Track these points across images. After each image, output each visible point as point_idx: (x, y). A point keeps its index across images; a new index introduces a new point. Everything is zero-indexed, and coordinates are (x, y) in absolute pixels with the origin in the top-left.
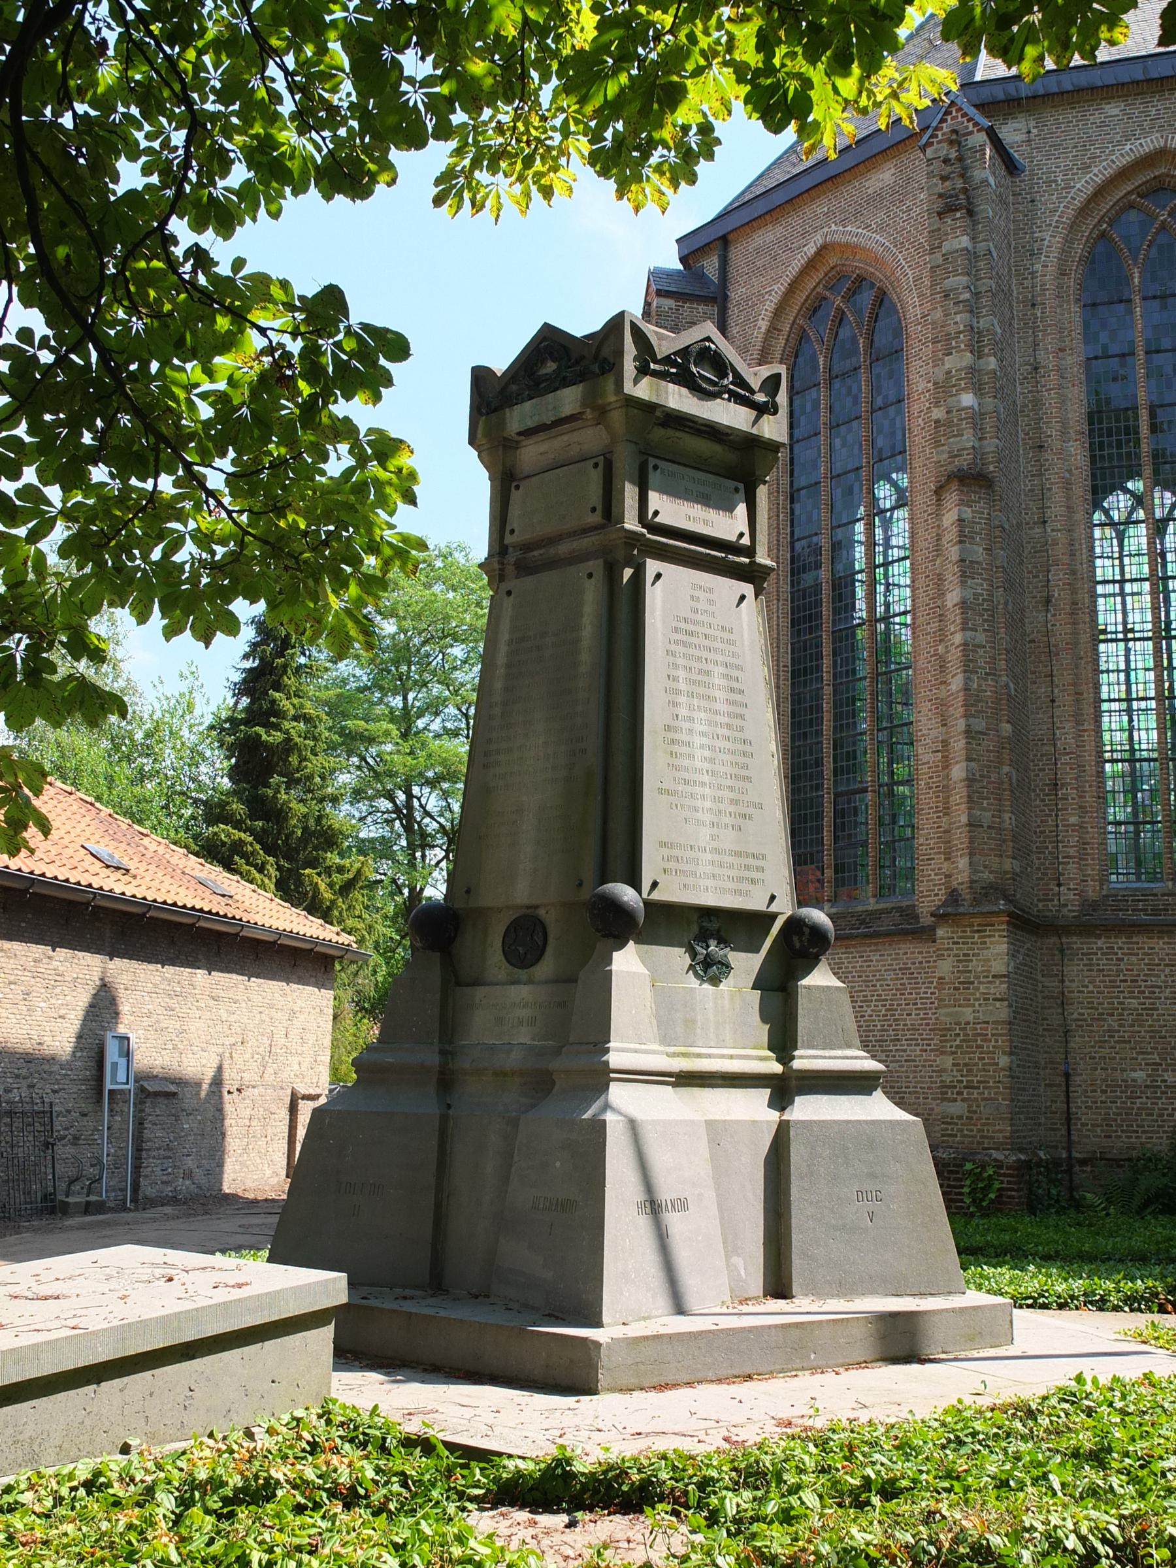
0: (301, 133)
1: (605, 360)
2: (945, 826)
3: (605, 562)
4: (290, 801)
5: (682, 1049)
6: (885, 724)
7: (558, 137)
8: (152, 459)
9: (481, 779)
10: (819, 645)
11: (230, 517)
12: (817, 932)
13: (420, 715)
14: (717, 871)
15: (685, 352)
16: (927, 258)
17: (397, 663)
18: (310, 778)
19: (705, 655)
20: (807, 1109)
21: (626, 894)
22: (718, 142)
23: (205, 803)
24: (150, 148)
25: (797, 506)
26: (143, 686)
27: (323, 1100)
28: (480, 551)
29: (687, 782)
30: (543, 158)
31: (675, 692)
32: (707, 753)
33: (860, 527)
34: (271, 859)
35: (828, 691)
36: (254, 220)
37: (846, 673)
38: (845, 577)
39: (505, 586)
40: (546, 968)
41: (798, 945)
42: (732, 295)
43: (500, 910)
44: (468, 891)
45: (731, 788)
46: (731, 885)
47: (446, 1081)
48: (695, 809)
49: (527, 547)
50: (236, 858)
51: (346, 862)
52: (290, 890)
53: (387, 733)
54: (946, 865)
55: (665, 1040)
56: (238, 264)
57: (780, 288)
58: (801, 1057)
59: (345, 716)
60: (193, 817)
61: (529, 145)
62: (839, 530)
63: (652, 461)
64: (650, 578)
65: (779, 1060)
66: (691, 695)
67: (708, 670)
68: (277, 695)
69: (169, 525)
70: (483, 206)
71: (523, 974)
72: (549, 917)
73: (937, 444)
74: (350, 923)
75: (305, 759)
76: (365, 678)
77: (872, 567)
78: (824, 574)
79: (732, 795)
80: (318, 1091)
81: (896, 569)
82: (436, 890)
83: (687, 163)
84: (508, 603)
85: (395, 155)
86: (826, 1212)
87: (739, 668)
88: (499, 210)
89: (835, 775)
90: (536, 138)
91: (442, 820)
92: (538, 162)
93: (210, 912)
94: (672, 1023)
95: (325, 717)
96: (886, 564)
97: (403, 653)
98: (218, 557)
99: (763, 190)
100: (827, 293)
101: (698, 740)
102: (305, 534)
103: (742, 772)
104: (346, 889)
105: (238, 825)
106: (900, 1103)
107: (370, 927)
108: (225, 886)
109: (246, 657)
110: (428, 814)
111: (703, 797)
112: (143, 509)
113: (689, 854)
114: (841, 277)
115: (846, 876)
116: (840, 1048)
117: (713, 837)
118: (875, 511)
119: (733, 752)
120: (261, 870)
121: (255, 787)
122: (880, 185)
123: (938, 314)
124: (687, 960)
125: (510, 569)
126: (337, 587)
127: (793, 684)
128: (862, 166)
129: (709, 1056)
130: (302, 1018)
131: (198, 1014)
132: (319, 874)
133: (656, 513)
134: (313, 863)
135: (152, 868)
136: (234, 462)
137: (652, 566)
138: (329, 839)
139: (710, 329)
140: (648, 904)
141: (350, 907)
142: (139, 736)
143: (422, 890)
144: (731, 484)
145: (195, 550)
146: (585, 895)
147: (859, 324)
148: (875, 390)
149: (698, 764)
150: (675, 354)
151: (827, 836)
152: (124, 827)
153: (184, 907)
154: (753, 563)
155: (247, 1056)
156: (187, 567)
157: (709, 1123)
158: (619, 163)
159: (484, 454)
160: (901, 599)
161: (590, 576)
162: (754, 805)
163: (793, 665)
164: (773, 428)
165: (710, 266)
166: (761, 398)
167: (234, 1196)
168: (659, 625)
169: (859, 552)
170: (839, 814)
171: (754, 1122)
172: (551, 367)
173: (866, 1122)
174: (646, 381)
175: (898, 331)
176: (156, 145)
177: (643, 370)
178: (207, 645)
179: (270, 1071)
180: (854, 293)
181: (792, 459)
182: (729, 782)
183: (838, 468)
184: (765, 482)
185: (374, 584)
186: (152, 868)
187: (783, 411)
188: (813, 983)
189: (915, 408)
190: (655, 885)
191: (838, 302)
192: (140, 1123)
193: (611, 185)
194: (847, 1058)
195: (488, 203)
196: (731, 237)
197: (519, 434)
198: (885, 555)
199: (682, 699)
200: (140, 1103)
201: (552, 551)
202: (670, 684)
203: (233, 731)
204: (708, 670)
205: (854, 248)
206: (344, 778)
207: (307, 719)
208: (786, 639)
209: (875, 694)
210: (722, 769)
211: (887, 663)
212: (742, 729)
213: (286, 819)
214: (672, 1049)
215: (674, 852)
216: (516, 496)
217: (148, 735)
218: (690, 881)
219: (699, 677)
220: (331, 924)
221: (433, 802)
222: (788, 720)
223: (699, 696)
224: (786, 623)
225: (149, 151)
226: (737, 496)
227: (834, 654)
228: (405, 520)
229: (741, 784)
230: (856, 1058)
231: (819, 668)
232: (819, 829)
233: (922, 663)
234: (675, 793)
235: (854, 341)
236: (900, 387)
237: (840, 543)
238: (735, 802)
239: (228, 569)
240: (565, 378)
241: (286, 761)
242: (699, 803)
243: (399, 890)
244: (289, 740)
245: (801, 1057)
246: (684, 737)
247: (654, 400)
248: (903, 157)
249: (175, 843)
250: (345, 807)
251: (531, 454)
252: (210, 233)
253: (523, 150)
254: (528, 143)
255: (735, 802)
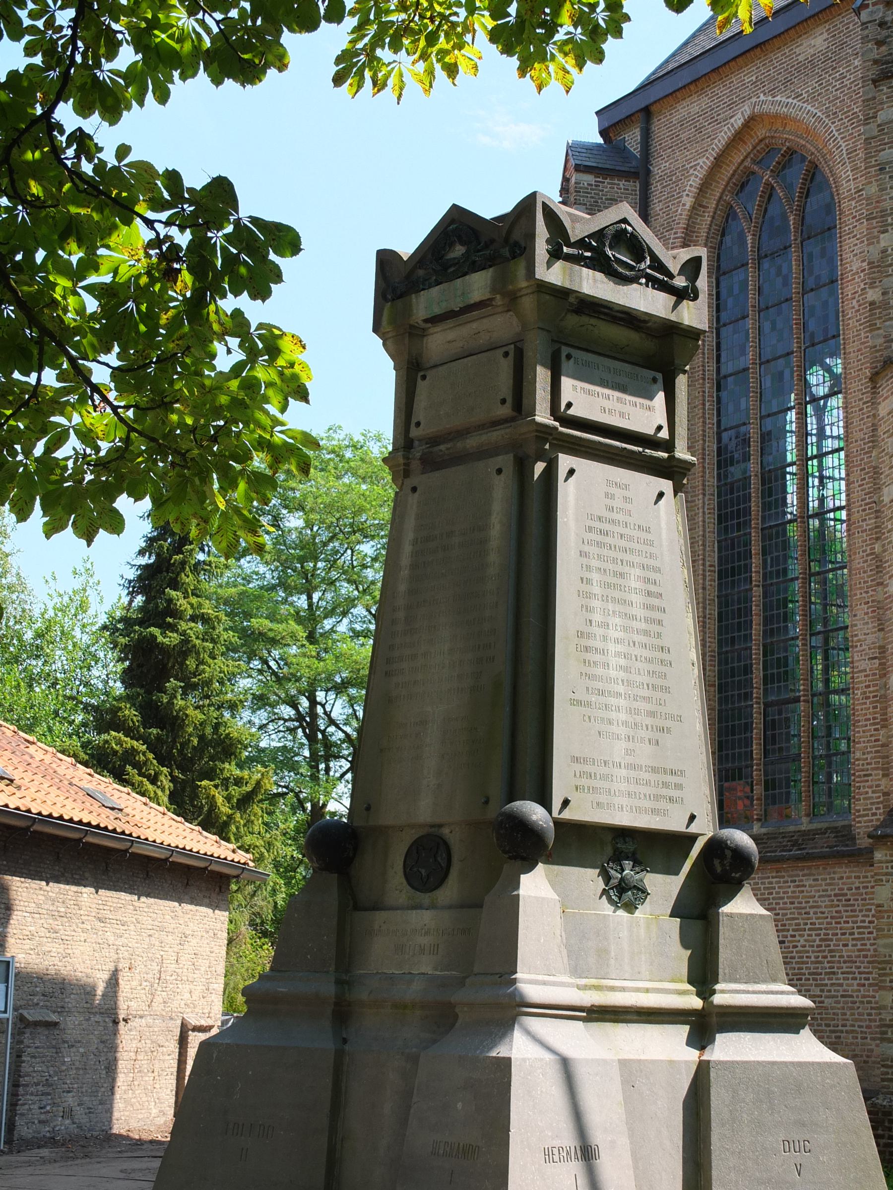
0: (191, 13)
1: (516, 244)
2: (883, 740)
3: (515, 456)
4: (187, 707)
5: (593, 981)
6: (819, 628)
7: (463, 13)
8: (36, 352)
9: (381, 685)
10: (748, 543)
11: (116, 413)
12: (739, 856)
13: (328, 614)
14: (632, 788)
15: (599, 235)
16: (862, 128)
17: (302, 560)
18: (208, 683)
19: (620, 555)
20: (729, 1048)
21: (536, 813)
22: (627, 18)
23: (96, 709)
24: (33, 26)
25: (724, 394)
26: (34, 583)
27: (214, 1031)
28: (388, 444)
29: (601, 693)
30: (447, 35)
31: (589, 596)
32: (622, 662)
33: (792, 416)
34: (165, 770)
35: (757, 592)
36: (141, 104)
37: (776, 574)
38: (776, 470)
39: (409, 483)
40: (449, 892)
41: (719, 869)
42: (655, 170)
43: (401, 829)
44: (368, 809)
45: (647, 699)
46: (648, 804)
47: (342, 1014)
48: (610, 722)
49: (434, 441)
50: (129, 768)
51: (246, 774)
52: (185, 803)
53: (293, 636)
54: (884, 782)
55: (576, 971)
56: (123, 151)
57: (705, 163)
58: (723, 992)
59: (248, 616)
60: (84, 724)
61: (432, 22)
62: (769, 420)
63: (565, 351)
64: (562, 473)
65: (699, 994)
66: (605, 599)
67: (625, 569)
68: (173, 593)
69: (52, 419)
70: (385, 85)
71: (425, 898)
72: (455, 837)
73: (872, 327)
74: (248, 840)
75: (202, 662)
76: (268, 576)
77: (804, 459)
78: (753, 467)
79: (649, 707)
80: (210, 1022)
81: (829, 461)
82: (339, 803)
83: (594, 41)
84: (413, 500)
85: (288, 39)
86: (750, 1163)
87: (657, 570)
88: (401, 89)
89: (765, 683)
90: (440, 14)
91: (348, 729)
92: (442, 39)
93: (98, 827)
94: (584, 953)
95: (224, 618)
96: (820, 456)
97: (310, 550)
98: (102, 453)
99: (676, 65)
100: (756, 168)
101: (612, 648)
102: (193, 430)
103: (659, 682)
104: (244, 802)
105: (130, 732)
106: (834, 1047)
107: (269, 844)
108: (115, 798)
109: (142, 552)
110: (332, 722)
111: (618, 709)
112: (26, 404)
113: (603, 770)
114: (771, 150)
115: (777, 791)
116: (764, 981)
117: (629, 752)
118: (806, 398)
119: (649, 661)
120: (154, 780)
121: (149, 692)
122: (812, 51)
123: (873, 189)
124: (601, 885)
125: (415, 465)
126: (225, 485)
127: (720, 585)
128: (792, 32)
129: (623, 989)
130: (194, 942)
131: (83, 936)
132: (216, 786)
133: (569, 405)
134: (210, 774)
135: (38, 778)
136: (119, 357)
137: (565, 461)
138: (227, 748)
139: (626, 210)
140: (558, 823)
141: (249, 823)
142: (29, 635)
143: (324, 805)
144: (651, 374)
145: (79, 446)
146: (492, 813)
147: (790, 200)
148: (806, 267)
149: (613, 673)
150: (589, 236)
151: (756, 749)
152: (9, 733)
153: (71, 820)
154: (672, 458)
155: (134, 983)
156: (70, 464)
157: (624, 1064)
158: (523, 39)
159: (389, 343)
160: (837, 493)
161: (499, 471)
162: (672, 717)
163: (720, 564)
164: (694, 315)
165: (632, 139)
166: (680, 282)
167: (121, 1136)
168: (572, 524)
169: (791, 441)
170: (769, 725)
171: (671, 1062)
172: (459, 251)
173: (792, 1063)
174: (559, 265)
175: (830, 208)
176: (40, 24)
177: (555, 254)
178: (89, 542)
179: (158, 999)
180: (784, 168)
181: (718, 345)
182: (646, 693)
183: (767, 354)
184: (685, 372)
185: (261, 484)
186: (38, 778)
187: (703, 297)
188: (735, 911)
189: (849, 290)
190: (566, 803)
191: (767, 176)
192: (18, 1056)
193: (514, 62)
194: (772, 993)
195: (390, 82)
196: (653, 108)
197: (426, 321)
198: (819, 446)
199: (596, 603)
200: (18, 1033)
201: (459, 445)
202: (584, 587)
203: (126, 633)
204: (625, 569)
205: (784, 119)
206: (244, 683)
207: (205, 619)
208: (712, 538)
209: (807, 595)
210: (639, 679)
211: (822, 562)
212: (659, 635)
213: (182, 726)
214: (583, 981)
215: (588, 768)
216: (422, 386)
217: (39, 635)
218: (603, 798)
219: (614, 580)
220: (228, 840)
221: (339, 708)
222: (713, 625)
223: (614, 600)
224: (712, 520)
225: (32, 30)
226: (655, 387)
227: (764, 553)
228: (297, 418)
229: (659, 695)
230: (782, 993)
231: (747, 568)
232: (748, 742)
233: (858, 563)
234: (589, 704)
235: (785, 218)
236: (834, 269)
237: (769, 433)
238: (652, 714)
239: (113, 466)
240: (474, 262)
241: (182, 663)
242: (613, 715)
243: (301, 803)
244: (186, 641)
245: (723, 992)
246: (598, 644)
247: (567, 285)
248: (837, 21)
249: (63, 752)
250: (246, 714)
251: (439, 342)
252: (96, 117)
253: (426, 27)
254: (432, 19)
255: (652, 714)
